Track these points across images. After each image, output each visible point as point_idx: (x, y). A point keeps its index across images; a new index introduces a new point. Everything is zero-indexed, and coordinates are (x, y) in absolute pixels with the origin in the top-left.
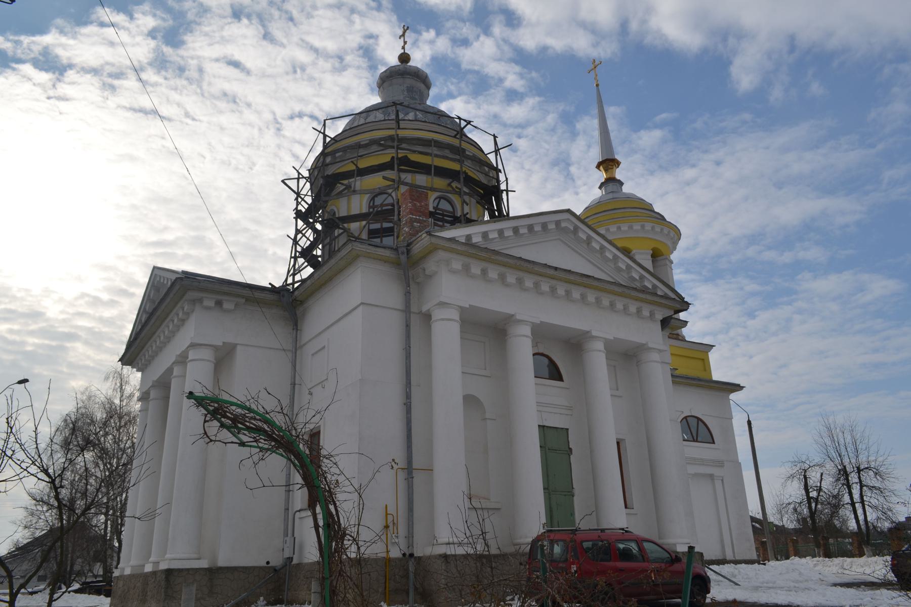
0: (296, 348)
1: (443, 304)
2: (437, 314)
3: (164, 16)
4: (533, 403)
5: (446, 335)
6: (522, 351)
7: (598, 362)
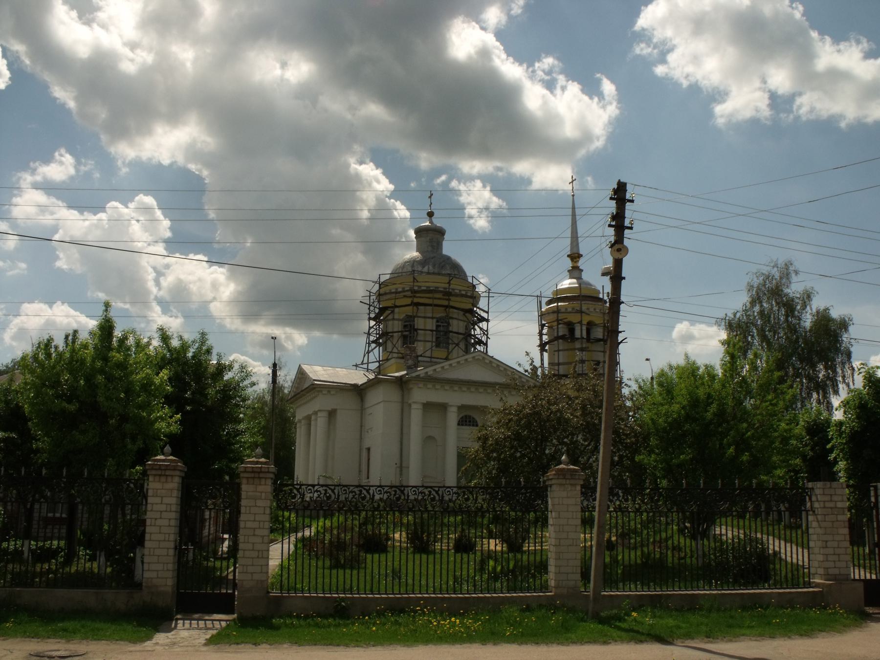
0: (362, 410)
1: (414, 402)
2: (414, 406)
5: (416, 414)
6: (453, 417)
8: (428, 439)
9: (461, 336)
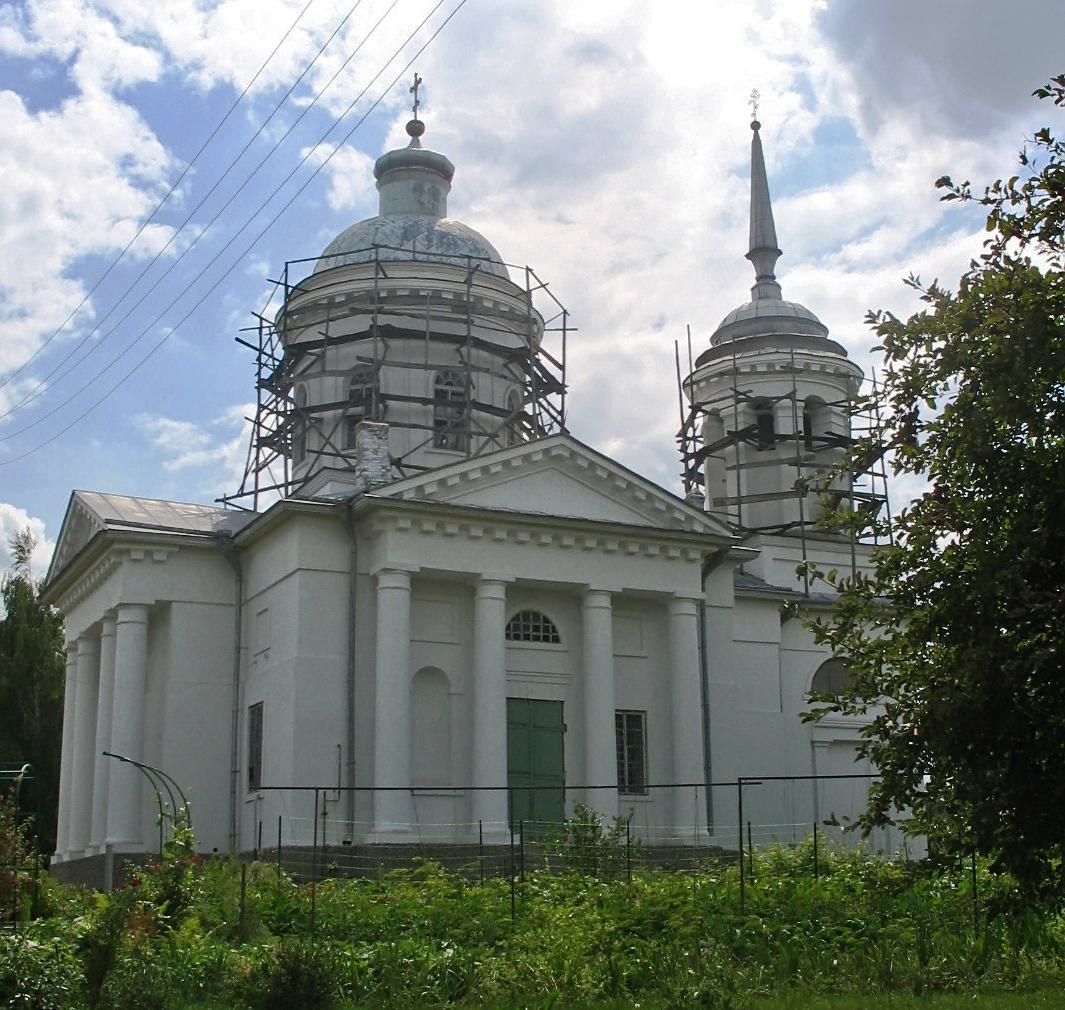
0: (241, 603)
1: (386, 571)
2: (385, 581)
3: (75, 735)
4: (498, 669)
5: (393, 604)
6: (493, 614)
7: (600, 618)
8: (427, 675)
9: (499, 420)
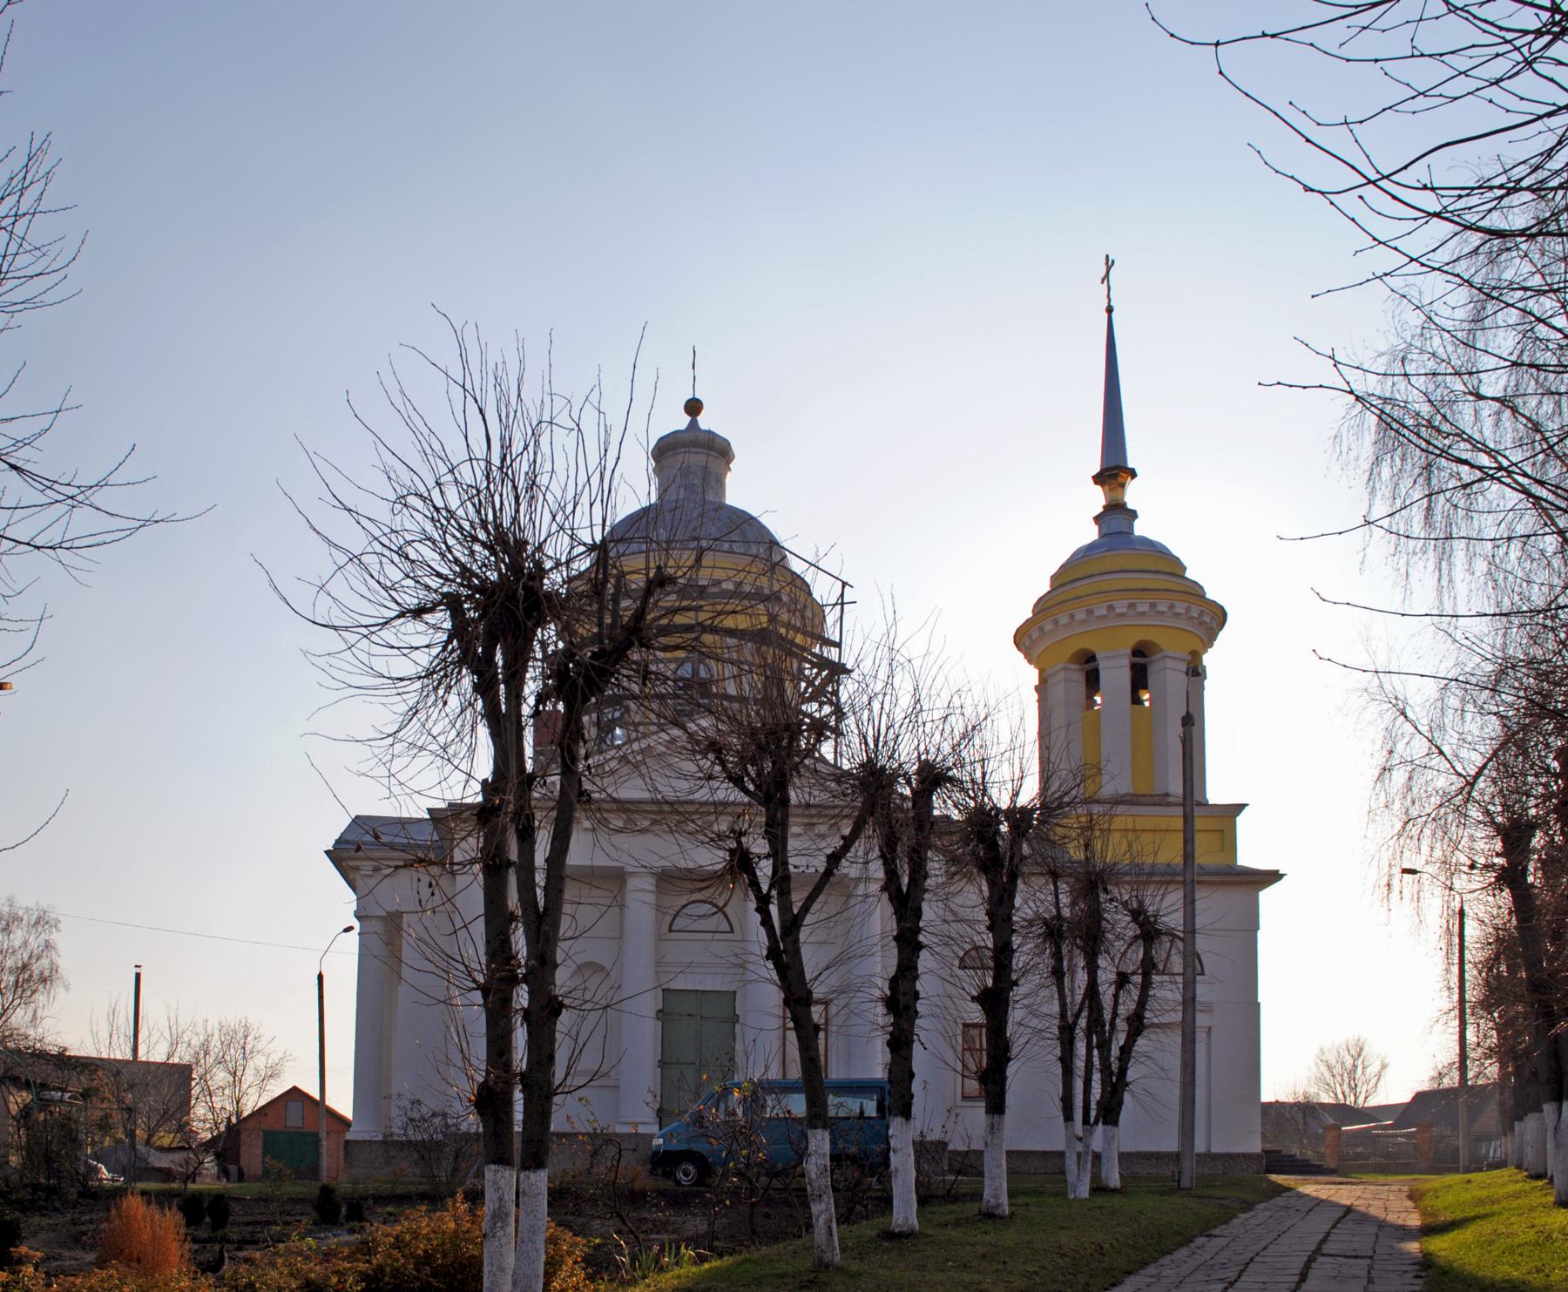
6: (641, 891)
7: (641, 891)
